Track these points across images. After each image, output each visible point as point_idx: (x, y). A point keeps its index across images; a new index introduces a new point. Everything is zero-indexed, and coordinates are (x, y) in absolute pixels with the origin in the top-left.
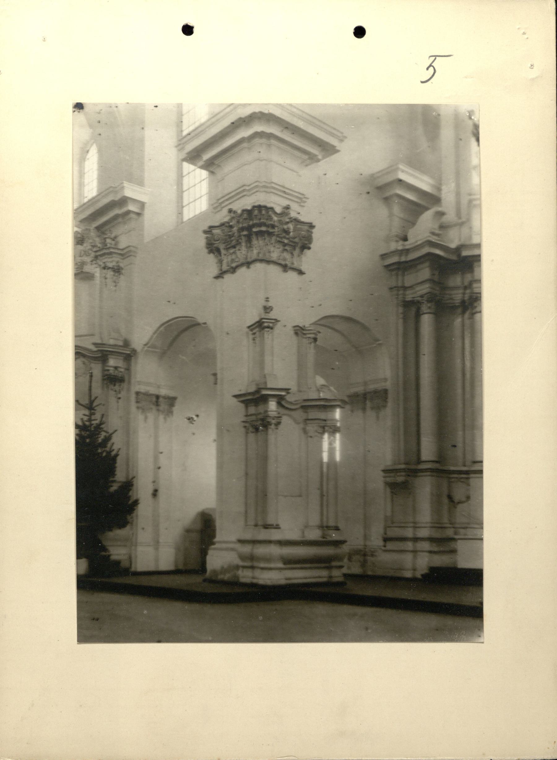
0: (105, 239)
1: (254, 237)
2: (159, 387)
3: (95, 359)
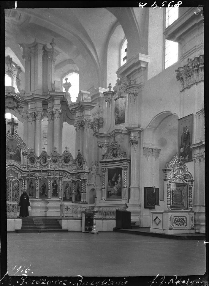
0: (130, 81)
1: (200, 69)
2: (153, 145)
3: (126, 134)
